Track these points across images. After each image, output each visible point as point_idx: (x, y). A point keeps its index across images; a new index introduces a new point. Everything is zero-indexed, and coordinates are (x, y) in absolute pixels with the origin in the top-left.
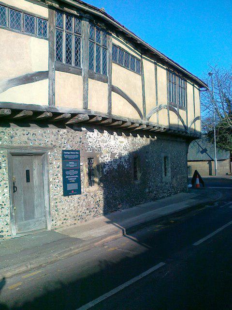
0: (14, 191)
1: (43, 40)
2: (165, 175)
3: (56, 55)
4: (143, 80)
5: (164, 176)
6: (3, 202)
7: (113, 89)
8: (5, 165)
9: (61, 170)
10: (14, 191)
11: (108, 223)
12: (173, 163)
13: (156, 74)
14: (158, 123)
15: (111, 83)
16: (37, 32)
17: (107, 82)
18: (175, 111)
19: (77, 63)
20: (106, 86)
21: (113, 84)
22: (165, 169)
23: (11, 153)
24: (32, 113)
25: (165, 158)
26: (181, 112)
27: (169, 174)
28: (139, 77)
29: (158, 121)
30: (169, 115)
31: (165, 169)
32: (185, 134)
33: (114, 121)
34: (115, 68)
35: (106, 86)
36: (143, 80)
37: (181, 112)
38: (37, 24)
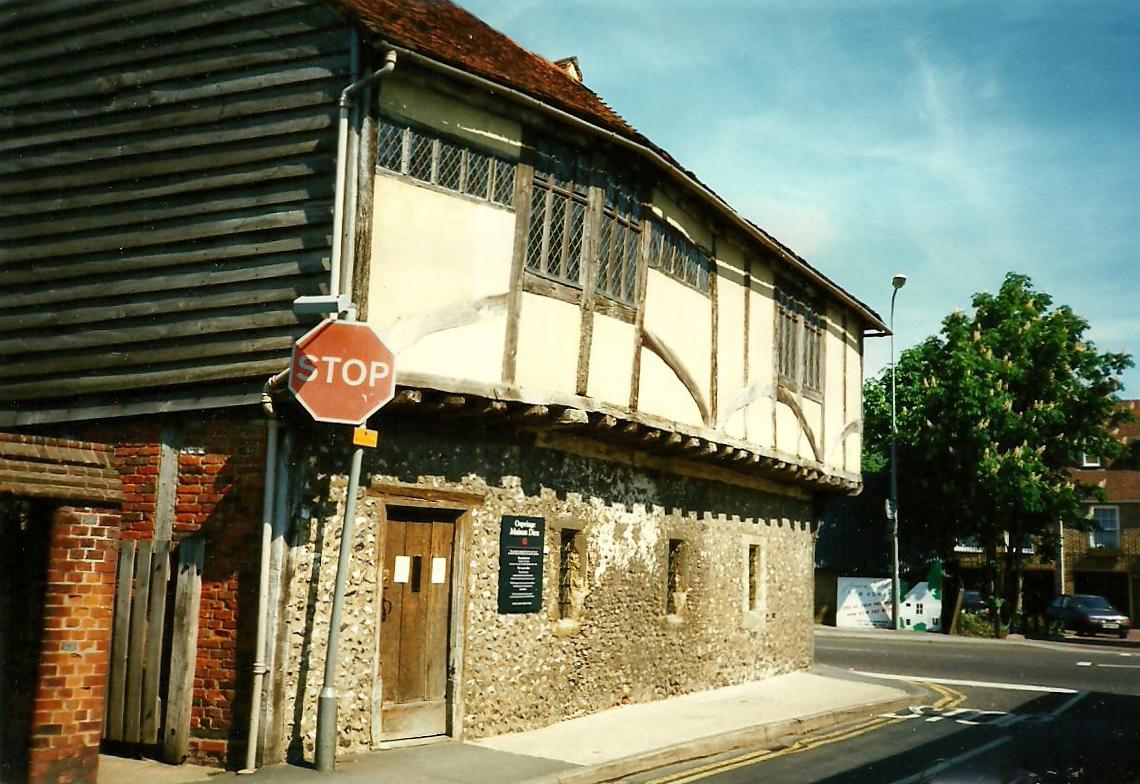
0: (347, 626)
1: (504, 212)
2: (752, 607)
3: (530, 251)
4: (714, 310)
5: (746, 607)
6: (360, 643)
7: (646, 341)
8: (373, 539)
9: (495, 561)
10: (347, 626)
11: (1130, 356)
12: (774, 568)
13: (747, 307)
14: (775, 448)
15: (642, 323)
16: (491, 192)
17: (633, 321)
18: (790, 403)
19: (573, 275)
20: (630, 332)
21: (647, 327)
22: (752, 587)
23: (389, 508)
24: (463, 400)
25: (753, 550)
26: (809, 407)
27: (761, 603)
28: (705, 303)
29: (746, 433)
30: (637, 370)
31: (752, 587)
32: (815, 475)
33: (644, 429)
34: (330, 75)
35: (630, 332)
36: (714, 310)
37: (809, 407)
38: (493, 171)
